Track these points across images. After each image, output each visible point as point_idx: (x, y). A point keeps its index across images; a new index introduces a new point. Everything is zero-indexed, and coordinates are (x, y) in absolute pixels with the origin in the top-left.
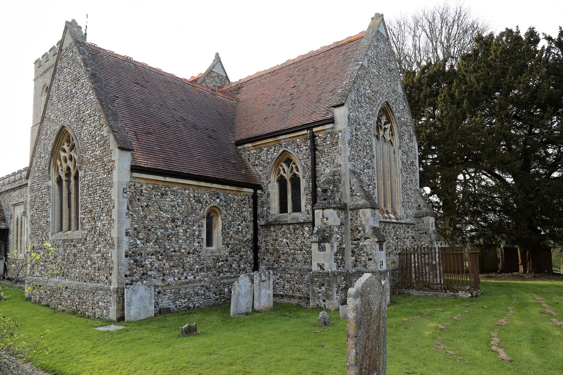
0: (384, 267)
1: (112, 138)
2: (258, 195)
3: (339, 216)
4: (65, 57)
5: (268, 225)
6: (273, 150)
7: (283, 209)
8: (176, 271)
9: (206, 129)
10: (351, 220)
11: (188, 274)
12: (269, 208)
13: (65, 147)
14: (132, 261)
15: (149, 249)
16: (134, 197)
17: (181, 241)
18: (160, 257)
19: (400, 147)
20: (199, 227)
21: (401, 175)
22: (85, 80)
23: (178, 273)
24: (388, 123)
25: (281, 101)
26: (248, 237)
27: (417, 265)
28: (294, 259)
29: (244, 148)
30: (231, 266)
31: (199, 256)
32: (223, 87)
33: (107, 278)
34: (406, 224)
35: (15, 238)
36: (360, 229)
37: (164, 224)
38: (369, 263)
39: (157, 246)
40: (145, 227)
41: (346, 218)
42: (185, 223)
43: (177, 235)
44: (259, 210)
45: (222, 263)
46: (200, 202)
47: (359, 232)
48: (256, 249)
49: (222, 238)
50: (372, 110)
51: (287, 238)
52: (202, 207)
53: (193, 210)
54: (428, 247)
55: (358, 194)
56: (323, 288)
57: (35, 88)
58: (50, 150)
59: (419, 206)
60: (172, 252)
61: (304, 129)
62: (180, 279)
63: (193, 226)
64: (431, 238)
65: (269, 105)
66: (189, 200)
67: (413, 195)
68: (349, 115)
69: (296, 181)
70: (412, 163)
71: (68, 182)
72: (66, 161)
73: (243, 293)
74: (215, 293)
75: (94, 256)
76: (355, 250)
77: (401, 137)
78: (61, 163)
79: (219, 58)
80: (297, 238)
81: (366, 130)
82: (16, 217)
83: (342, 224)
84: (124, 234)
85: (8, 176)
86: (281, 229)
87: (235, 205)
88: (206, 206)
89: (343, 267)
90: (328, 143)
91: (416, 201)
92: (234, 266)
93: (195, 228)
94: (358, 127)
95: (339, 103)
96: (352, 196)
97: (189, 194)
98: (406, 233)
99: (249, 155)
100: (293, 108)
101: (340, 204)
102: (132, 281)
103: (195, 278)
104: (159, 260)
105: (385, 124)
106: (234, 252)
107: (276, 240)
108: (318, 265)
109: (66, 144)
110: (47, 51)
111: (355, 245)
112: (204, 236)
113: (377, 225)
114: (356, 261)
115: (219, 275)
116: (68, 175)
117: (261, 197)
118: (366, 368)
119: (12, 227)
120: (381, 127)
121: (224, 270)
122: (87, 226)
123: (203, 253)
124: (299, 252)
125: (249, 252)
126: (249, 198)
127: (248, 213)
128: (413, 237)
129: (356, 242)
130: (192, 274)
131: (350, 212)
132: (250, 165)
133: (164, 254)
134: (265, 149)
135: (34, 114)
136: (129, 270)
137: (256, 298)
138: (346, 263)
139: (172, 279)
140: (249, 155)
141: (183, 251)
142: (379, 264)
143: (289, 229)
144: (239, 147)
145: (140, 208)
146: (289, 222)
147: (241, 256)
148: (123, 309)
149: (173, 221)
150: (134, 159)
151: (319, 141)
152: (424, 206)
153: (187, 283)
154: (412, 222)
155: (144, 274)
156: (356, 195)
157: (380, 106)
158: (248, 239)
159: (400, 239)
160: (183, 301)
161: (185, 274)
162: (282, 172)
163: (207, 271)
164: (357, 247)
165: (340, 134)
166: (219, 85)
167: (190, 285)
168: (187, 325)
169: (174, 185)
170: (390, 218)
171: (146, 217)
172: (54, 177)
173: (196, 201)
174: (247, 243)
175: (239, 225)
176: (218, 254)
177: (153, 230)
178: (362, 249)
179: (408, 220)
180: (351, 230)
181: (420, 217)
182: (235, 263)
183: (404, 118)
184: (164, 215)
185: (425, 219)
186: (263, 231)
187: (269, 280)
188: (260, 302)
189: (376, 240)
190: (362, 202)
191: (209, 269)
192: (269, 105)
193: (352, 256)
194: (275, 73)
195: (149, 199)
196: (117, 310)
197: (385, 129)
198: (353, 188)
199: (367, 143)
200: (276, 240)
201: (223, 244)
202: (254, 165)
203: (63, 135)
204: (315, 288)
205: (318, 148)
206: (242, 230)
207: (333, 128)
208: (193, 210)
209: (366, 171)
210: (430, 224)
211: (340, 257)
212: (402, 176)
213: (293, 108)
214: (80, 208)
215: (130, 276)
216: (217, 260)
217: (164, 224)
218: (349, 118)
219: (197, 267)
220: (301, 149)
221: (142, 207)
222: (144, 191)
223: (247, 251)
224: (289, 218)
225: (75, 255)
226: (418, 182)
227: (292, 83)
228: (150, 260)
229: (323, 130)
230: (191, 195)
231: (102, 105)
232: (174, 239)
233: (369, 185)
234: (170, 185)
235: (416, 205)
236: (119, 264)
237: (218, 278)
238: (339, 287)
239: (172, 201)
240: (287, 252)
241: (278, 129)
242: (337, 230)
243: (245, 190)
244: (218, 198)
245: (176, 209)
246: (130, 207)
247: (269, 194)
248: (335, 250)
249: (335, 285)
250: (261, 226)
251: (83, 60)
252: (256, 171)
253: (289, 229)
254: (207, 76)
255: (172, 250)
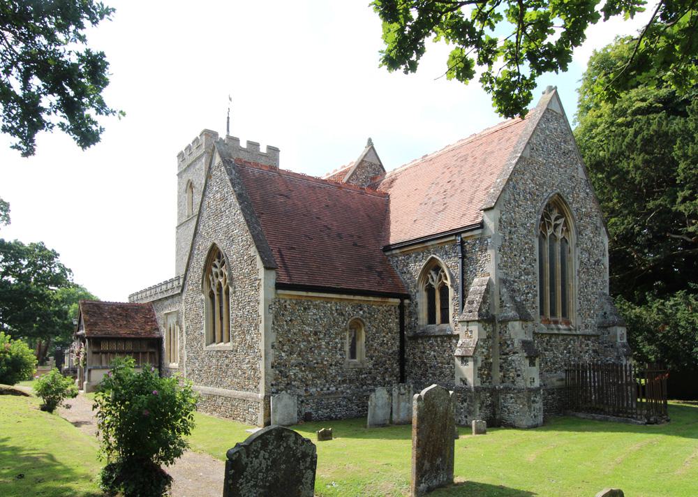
0: (537, 384)
1: (258, 258)
2: (405, 305)
3: (485, 329)
4: (214, 175)
5: (415, 337)
6: (421, 256)
7: (432, 319)
8: (319, 382)
9: (352, 236)
10: (500, 333)
11: (330, 385)
12: (417, 319)
13: (216, 262)
14: (277, 372)
15: (292, 361)
16: (278, 312)
17: (323, 354)
18: (303, 369)
19: (577, 245)
20: (341, 339)
21: (577, 277)
22: (233, 199)
23: (321, 384)
24: (562, 217)
25: (434, 199)
26: (394, 349)
27: (597, 384)
28: (441, 373)
29: (392, 255)
30: (375, 378)
31: (341, 368)
32: (376, 178)
33: (255, 387)
34: (584, 336)
35: (169, 347)
36: (509, 342)
37: (307, 337)
38: (519, 379)
39: (300, 358)
40: (289, 341)
41: (494, 331)
42: (327, 336)
43: (319, 347)
44: (407, 321)
45: (366, 375)
46: (342, 315)
47: (508, 346)
48: (402, 361)
49: (365, 350)
50: (534, 207)
51: (434, 351)
52: (345, 320)
53: (336, 324)
54: (614, 363)
55: (508, 305)
56: (465, 404)
57: (179, 183)
58: (203, 265)
59: (605, 313)
60: (315, 363)
61: (452, 235)
62: (322, 390)
63: (335, 338)
64: (618, 352)
65: (421, 204)
66: (332, 314)
67: (597, 301)
68: (501, 218)
69: (444, 290)
70: (598, 262)
71: (218, 298)
72: (217, 277)
73: (380, 405)
74: (357, 405)
75: (245, 366)
76: (503, 365)
77: (579, 233)
78: (213, 279)
79: (372, 144)
80: (445, 351)
81: (525, 232)
82: (169, 326)
83: (488, 337)
84: (270, 347)
85: (161, 285)
86: (428, 341)
87: (380, 316)
88: (349, 319)
89: (490, 382)
90: (477, 250)
91: (602, 308)
92: (378, 378)
93: (337, 340)
94: (513, 229)
95: (489, 207)
96: (501, 307)
97: (331, 307)
98: (583, 346)
99: (397, 262)
100: (445, 209)
101: (487, 316)
102: (278, 390)
103: (337, 389)
104: (302, 371)
105: (557, 219)
106: (378, 364)
107: (424, 353)
108: (461, 379)
109: (217, 260)
110: (190, 143)
111: (503, 359)
112: (347, 348)
113: (530, 339)
114: (504, 377)
115: (362, 388)
116: (220, 289)
117: (409, 307)
118: (429, 452)
119: (164, 333)
120: (550, 224)
121: (368, 382)
122: (238, 339)
123: (345, 366)
124: (446, 366)
125: (395, 365)
126: (395, 308)
127: (394, 324)
128: (595, 351)
129: (504, 357)
130: (334, 386)
131: (498, 325)
132: (399, 273)
133: (307, 365)
134: (413, 255)
135: (178, 213)
136: (275, 380)
137: (394, 410)
138: (494, 379)
139: (314, 390)
140: (397, 262)
141: (325, 363)
142: (529, 380)
143: (437, 341)
144: (387, 254)
145: (285, 323)
146: (437, 334)
147: (387, 369)
148: (270, 415)
149: (316, 334)
150: (278, 276)
151: (468, 248)
152: (611, 314)
153: (329, 394)
154: (594, 333)
155: (288, 384)
156: (506, 306)
157: (547, 200)
158: (394, 351)
159: (574, 353)
160: (325, 411)
161: (327, 386)
162: (430, 281)
163: (350, 383)
164: (505, 362)
165: (489, 240)
166: (371, 175)
167: (332, 396)
168: (323, 429)
169: (316, 299)
170: (559, 329)
171: (289, 330)
172: (207, 292)
173: (339, 314)
174: (393, 356)
175: (384, 337)
176: (361, 366)
177: (296, 343)
178: (511, 365)
179: (589, 331)
180: (500, 343)
181: (606, 327)
182: (379, 375)
183: (585, 208)
184: (307, 328)
185: (612, 330)
186: (411, 343)
187: (409, 393)
188: (398, 413)
189: (525, 355)
190: (512, 313)
191: (351, 381)
192: (421, 204)
193: (501, 371)
194: (432, 162)
195: (292, 313)
196: (265, 415)
197: (556, 226)
198: (503, 299)
199: (526, 246)
200: (424, 353)
201: (366, 357)
202: (402, 273)
203: (215, 254)
204: (457, 403)
205: (467, 255)
206: (387, 342)
207: (482, 234)
208: (336, 324)
209: (523, 278)
210: (618, 336)
211: (486, 372)
212: (580, 278)
213: (445, 209)
214: (231, 322)
215: (276, 385)
216: (360, 372)
217: (307, 337)
218: (500, 222)
219: (340, 379)
220: (450, 256)
221: (286, 321)
222: (288, 307)
223: (393, 363)
224: (437, 330)
225: (227, 365)
226: (608, 284)
227: (447, 176)
228: (294, 371)
229: (472, 236)
230: (334, 308)
231: (249, 226)
232: (316, 351)
233: (528, 293)
234: (313, 300)
235: (601, 313)
236: (266, 374)
237: (361, 390)
238: (483, 403)
239: (314, 314)
240: (435, 366)
241: (426, 235)
242: (482, 343)
243: (391, 300)
244: (361, 310)
245: (318, 322)
246: (275, 322)
247: (417, 304)
248: (479, 364)
249: (478, 402)
250: (408, 337)
251: (231, 180)
252: (404, 279)
253: (437, 341)
254: (358, 167)
255: (315, 361)
